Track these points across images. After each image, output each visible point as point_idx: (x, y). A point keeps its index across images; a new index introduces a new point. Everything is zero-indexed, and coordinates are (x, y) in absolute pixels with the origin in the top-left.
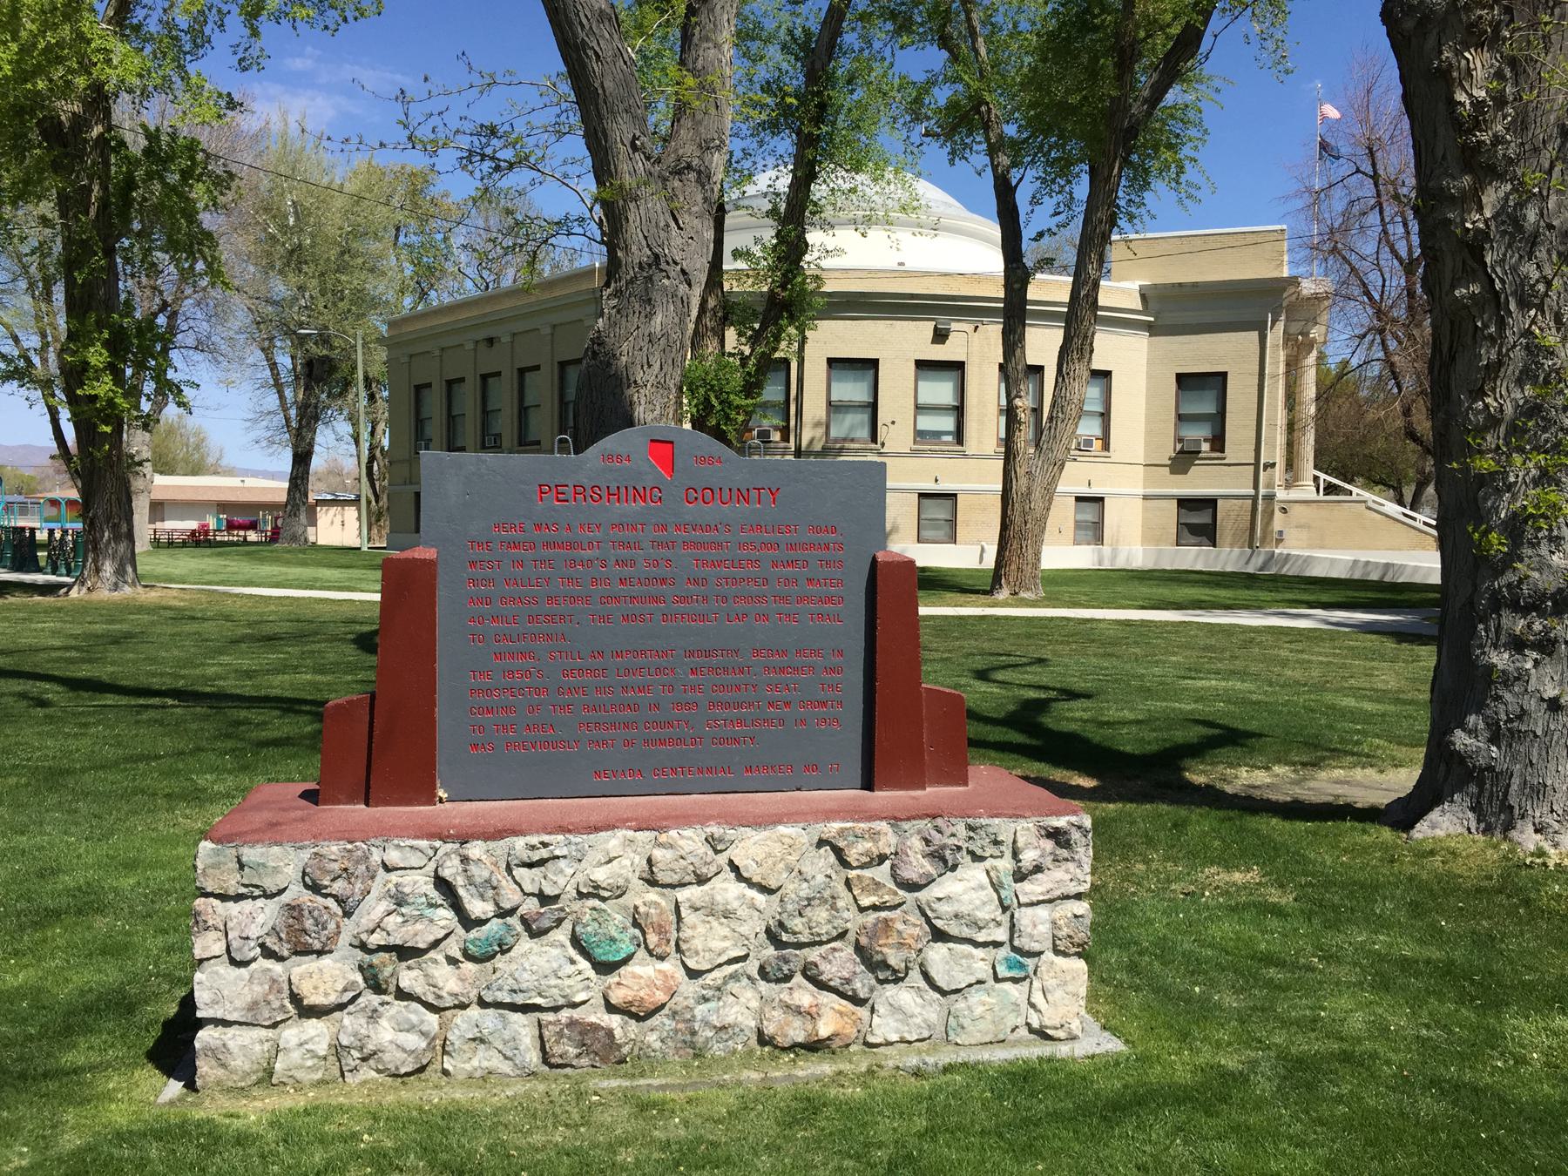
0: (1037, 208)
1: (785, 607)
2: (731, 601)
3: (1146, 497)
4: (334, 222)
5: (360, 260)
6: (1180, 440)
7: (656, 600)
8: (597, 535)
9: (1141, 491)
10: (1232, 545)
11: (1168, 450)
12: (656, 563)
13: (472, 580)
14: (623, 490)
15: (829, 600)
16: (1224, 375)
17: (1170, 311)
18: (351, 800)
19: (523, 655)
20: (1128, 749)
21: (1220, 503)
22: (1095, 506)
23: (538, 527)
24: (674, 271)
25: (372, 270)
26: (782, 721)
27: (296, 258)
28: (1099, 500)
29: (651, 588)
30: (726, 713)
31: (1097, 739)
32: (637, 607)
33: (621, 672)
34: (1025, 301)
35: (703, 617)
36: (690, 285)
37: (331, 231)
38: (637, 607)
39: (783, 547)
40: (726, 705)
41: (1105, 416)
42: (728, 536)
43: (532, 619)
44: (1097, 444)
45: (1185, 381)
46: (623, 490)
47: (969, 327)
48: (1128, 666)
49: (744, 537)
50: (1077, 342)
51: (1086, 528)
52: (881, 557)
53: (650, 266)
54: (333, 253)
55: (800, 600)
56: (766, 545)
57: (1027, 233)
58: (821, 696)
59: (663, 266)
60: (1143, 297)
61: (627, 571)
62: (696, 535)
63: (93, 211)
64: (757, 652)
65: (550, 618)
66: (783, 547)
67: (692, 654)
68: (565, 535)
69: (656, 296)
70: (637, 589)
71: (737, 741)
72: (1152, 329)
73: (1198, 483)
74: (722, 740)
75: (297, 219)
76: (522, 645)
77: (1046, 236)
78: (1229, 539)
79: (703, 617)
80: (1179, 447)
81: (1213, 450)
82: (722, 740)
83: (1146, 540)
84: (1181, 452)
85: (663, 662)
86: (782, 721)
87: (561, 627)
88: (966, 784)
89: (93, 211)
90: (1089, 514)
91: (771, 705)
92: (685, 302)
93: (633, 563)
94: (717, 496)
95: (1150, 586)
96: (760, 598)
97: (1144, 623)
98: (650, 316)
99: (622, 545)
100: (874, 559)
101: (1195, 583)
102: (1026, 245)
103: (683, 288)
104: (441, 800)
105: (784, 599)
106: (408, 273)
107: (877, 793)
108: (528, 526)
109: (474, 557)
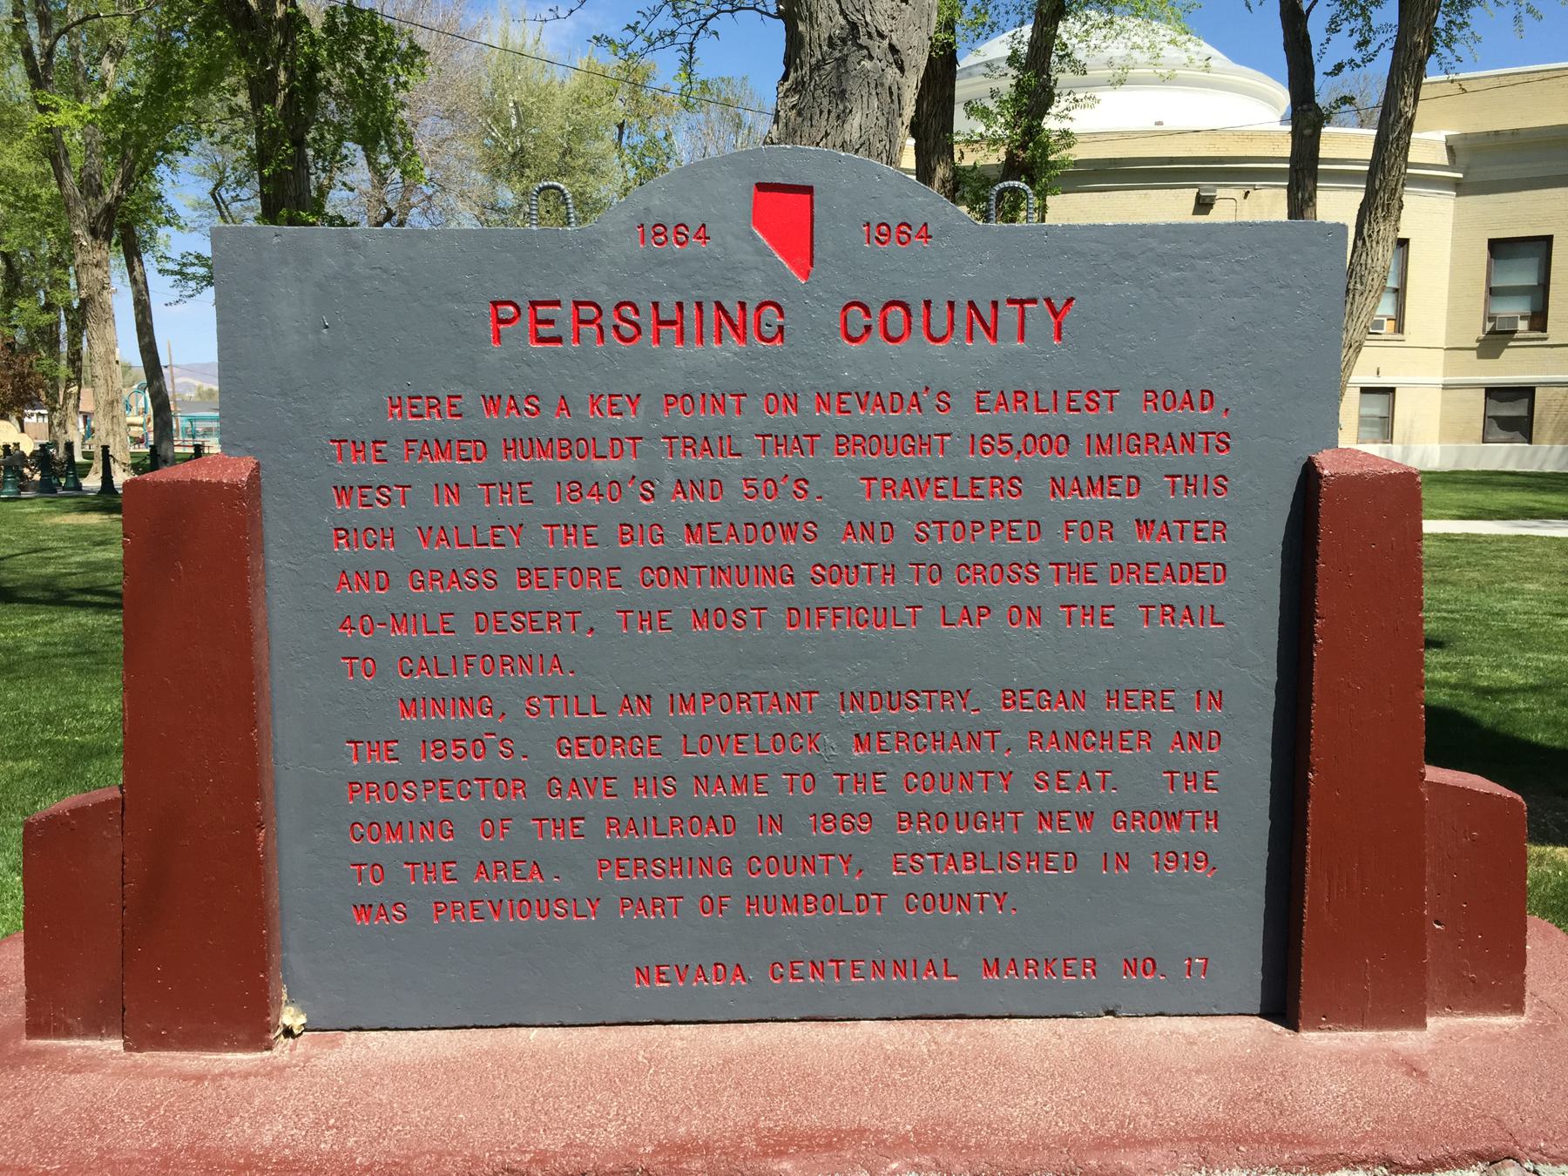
0: (1333, 37)
1: (1082, 591)
2: (949, 575)
3: (1446, 387)
4: (553, 124)
5: (581, 161)
6: (1491, 319)
7: (771, 573)
8: (630, 421)
9: (1441, 380)
10: (1552, 441)
11: (1475, 330)
12: (772, 487)
13: (341, 532)
14: (690, 311)
15: (1193, 571)
16: (1548, 240)
17: (1485, 165)
18: (94, 1028)
19: (466, 704)
20: (1540, 737)
21: (1538, 392)
22: (1384, 398)
23: (492, 403)
24: (879, 48)
25: (592, 171)
26: (1072, 859)
27: (519, 161)
28: (1390, 391)
29: (760, 546)
30: (939, 838)
31: (1487, 720)
32: (729, 594)
33: (693, 744)
34: (1316, 159)
35: (884, 616)
36: (902, 69)
37: (553, 132)
38: (729, 594)
39: (1079, 443)
40: (940, 819)
41: (1400, 293)
42: (944, 421)
43: (485, 620)
44: (1389, 326)
45: (1499, 248)
46: (690, 311)
47: (1237, 193)
48: (1475, 599)
49: (984, 423)
50: (1383, 196)
51: (1373, 424)
52: (1328, 466)
53: (844, 41)
54: (555, 156)
55: (1120, 571)
56: (1039, 442)
57: (1321, 67)
58: (1170, 800)
59: (863, 40)
60: (1450, 150)
61: (703, 508)
62: (866, 419)
63: (280, 100)
64: (1012, 697)
65: (528, 618)
66: (1079, 443)
67: (857, 700)
68: (553, 424)
69: (852, 86)
70: (728, 551)
71: (964, 902)
72: (1460, 188)
73: (1512, 369)
74: (929, 901)
75: (519, 120)
76: (458, 682)
77: (1347, 69)
78: (1549, 434)
79: (884, 616)
80: (1489, 326)
81: (1531, 329)
82: (929, 901)
83: (1444, 436)
84: (1493, 332)
85: (791, 719)
86: (1072, 859)
87: (552, 639)
88: (1517, 1007)
89: (280, 100)
90: (1376, 406)
91: (1044, 818)
92: (895, 95)
93: (716, 486)
94: (918, 322)
95: (1458, 490)
96: (1026, 570)
97: (1469, 538)
98: (843, 117)
99: (691, 443)
100: (1310, 472)
101: (1513, 486)
102: (1320, 81)
103: (892, 73)
104: (288, 1032)
105: (1082, 571)
106: (631, 175)
107: (1315, 1040)
108: (471, 401)
109: (347, 479)
